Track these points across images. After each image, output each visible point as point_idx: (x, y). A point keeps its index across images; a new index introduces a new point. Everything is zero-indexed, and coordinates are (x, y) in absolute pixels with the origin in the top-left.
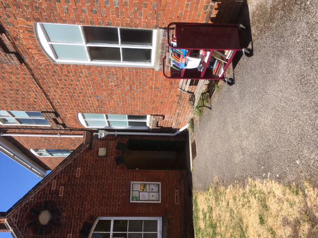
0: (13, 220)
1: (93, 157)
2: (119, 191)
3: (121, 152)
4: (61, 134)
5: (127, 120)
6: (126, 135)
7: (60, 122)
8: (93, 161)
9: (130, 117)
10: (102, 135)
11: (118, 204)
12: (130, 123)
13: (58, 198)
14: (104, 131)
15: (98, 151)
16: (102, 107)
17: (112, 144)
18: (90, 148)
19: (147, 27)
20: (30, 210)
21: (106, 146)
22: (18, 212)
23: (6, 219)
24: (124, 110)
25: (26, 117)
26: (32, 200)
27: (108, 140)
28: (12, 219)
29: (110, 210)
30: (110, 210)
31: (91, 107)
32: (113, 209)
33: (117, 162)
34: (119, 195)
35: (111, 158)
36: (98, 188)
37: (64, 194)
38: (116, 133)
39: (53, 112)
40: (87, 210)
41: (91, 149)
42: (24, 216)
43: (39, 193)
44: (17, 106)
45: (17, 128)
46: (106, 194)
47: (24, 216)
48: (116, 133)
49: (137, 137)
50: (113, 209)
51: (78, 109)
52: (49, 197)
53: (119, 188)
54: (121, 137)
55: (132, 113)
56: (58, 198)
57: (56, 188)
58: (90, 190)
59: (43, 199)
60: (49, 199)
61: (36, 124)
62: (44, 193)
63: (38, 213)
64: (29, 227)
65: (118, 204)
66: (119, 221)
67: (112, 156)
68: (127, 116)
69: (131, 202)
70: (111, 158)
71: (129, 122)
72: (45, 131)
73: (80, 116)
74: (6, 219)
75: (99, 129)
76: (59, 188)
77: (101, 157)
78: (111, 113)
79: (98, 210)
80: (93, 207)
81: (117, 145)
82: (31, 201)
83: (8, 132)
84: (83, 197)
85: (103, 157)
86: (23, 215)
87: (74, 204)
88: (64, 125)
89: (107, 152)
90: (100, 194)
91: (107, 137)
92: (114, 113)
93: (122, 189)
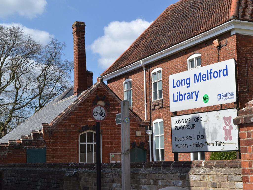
0: (99, 87)
1: (135, 128)
2: (116, 146)
3: (139, 145)
4: (147, 105)
5: (160, 149)
6: (149, 148)
7: (157, 107)
8: (132, 128)
9: (162, 150)
10: (149, 132)
11: (109, 146)
12: (158, 151)
13: (111, 110)
14: (151, 134)
15: (138, 131)
16: (168, 134)
17: (143, 139)
18: (141, 126)
19: (206, 158)
20: (104, 95)
21: (142, 136)
22: (104, 89)
23: (99, 82)
24: (167, 147)
25: (158, 89)
26: (110, 96)
27: (146, 136)
28: (100, 86)
29: (106, 141)
30: (106, 141)
31: (168, 128)
32: (107, 143)
33: (132, 143)
34: (114, 146)
35: (134, 140)
36: (118, 133)
37: (113, 113)
38: (150, 141)
39: (163, 106)
40: (105, 128)
41: (139, 126)
42: (101, 93)
43: (114, 99)
44: (166, 88)
45: (150, 84)
46: (114, 138)
47: (101, 93)
48: (150, 141)
49: (148, 155)
50: (107, 143)
51: (166, 121)
52: (112, 105)
53: (117, 146)
54: (148, 144)
55: (166, 151)
56: (111, 110)
57: (117, 108)
58: (117, 128)
59: (111, 102)
60: (111, 105)
61: (154, 92)
62: (113, 102)
63: (103, 100)
64: (96, 96)
65: (109, 146)
66: (16, 146)
67: (136, 140)
68: (163, 148)
69: (111, 154)
70: (134, 140)
71: (159, 150)
72: (148, 96)
73: (161, 120)
74: (99, 82)
75: (152, 130)
76: (117, 110)
77: (135, 133)
78: (165, 139)
79: (106, 135)
80: (107, 131)
81: (143, 143)
82: (109, 95)
83: (146, 71)
84: (88, 113)
85: (135, 135)
86: (102, 92)
87: (109, 120)
88: (154, 109)
89: (138, 136)
90: (114, 135)
91: (147, 136)
92: (164, 141)
93: (117, 148)
